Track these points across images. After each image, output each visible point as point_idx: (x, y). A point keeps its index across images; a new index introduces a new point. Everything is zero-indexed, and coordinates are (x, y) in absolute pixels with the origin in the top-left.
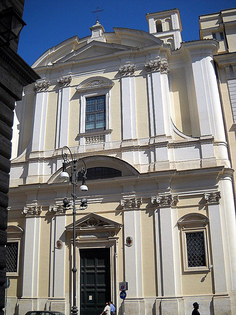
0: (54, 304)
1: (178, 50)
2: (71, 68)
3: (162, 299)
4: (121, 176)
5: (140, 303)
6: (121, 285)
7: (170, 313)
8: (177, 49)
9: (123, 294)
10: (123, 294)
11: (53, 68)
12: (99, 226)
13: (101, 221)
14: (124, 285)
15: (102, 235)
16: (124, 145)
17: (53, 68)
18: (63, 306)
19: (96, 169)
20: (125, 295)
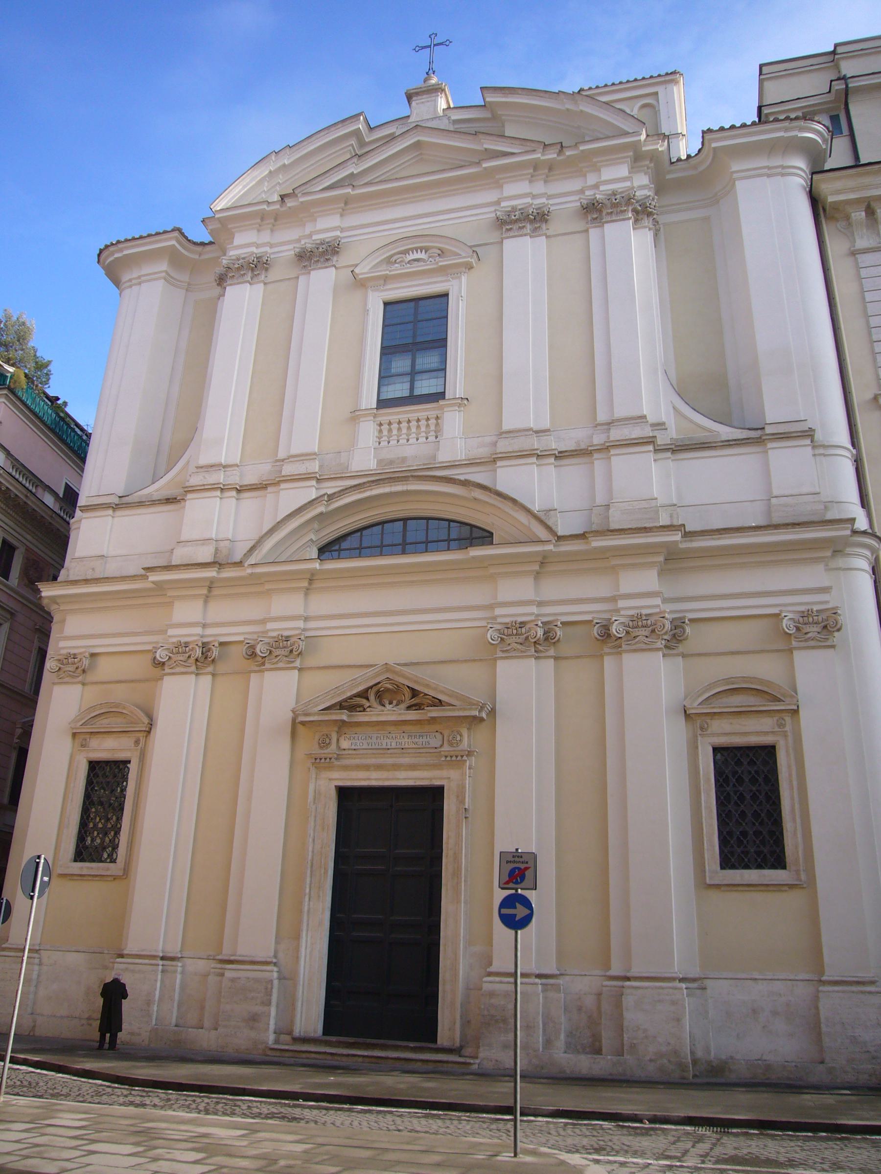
0: (233, 980)
1: (690, 160)
2: (340, 210)
3: (628, 983)
4: (491, 543)
5: (544, 991)
6: (507, 862)
7: (655, 1037)
8: (689, 157)
9: (515, 908)
10: (515, 908)
11: (284, 209)
12: (409, 708)
13: (414, 693)
14: (522, 866)
15: (417, 740)
16: (504, 446)
17: (284, 209)
18: (266, 989)
19: (421, 303)
20: (527, 912)
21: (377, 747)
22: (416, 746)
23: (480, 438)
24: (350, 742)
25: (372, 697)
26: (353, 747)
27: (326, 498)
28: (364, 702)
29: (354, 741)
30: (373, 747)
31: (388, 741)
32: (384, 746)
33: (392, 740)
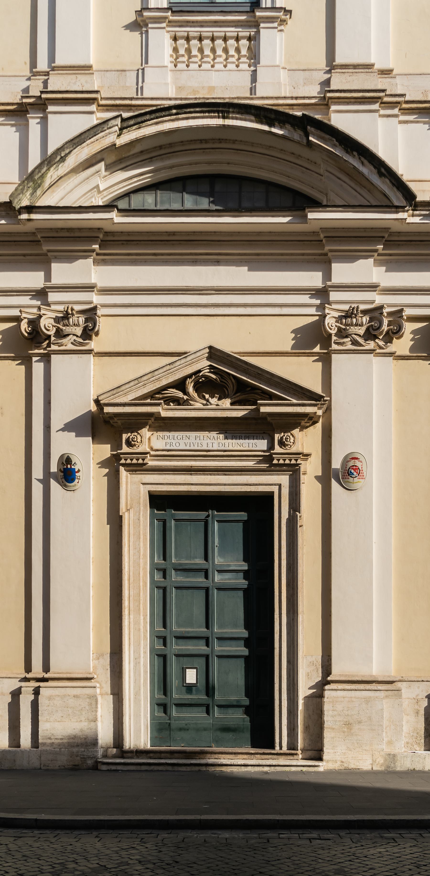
21: (196, 448)
22: (242, 448)
23: (307, 73)
24: (164, 441)
25: (190, 389)
26: (168, 447)
27: (118, 121)
28: (180, 394)
29: (168, 441)
30: (192, 448)
31: (209, 441)
32: (205, 448)
33: (213, 441)
